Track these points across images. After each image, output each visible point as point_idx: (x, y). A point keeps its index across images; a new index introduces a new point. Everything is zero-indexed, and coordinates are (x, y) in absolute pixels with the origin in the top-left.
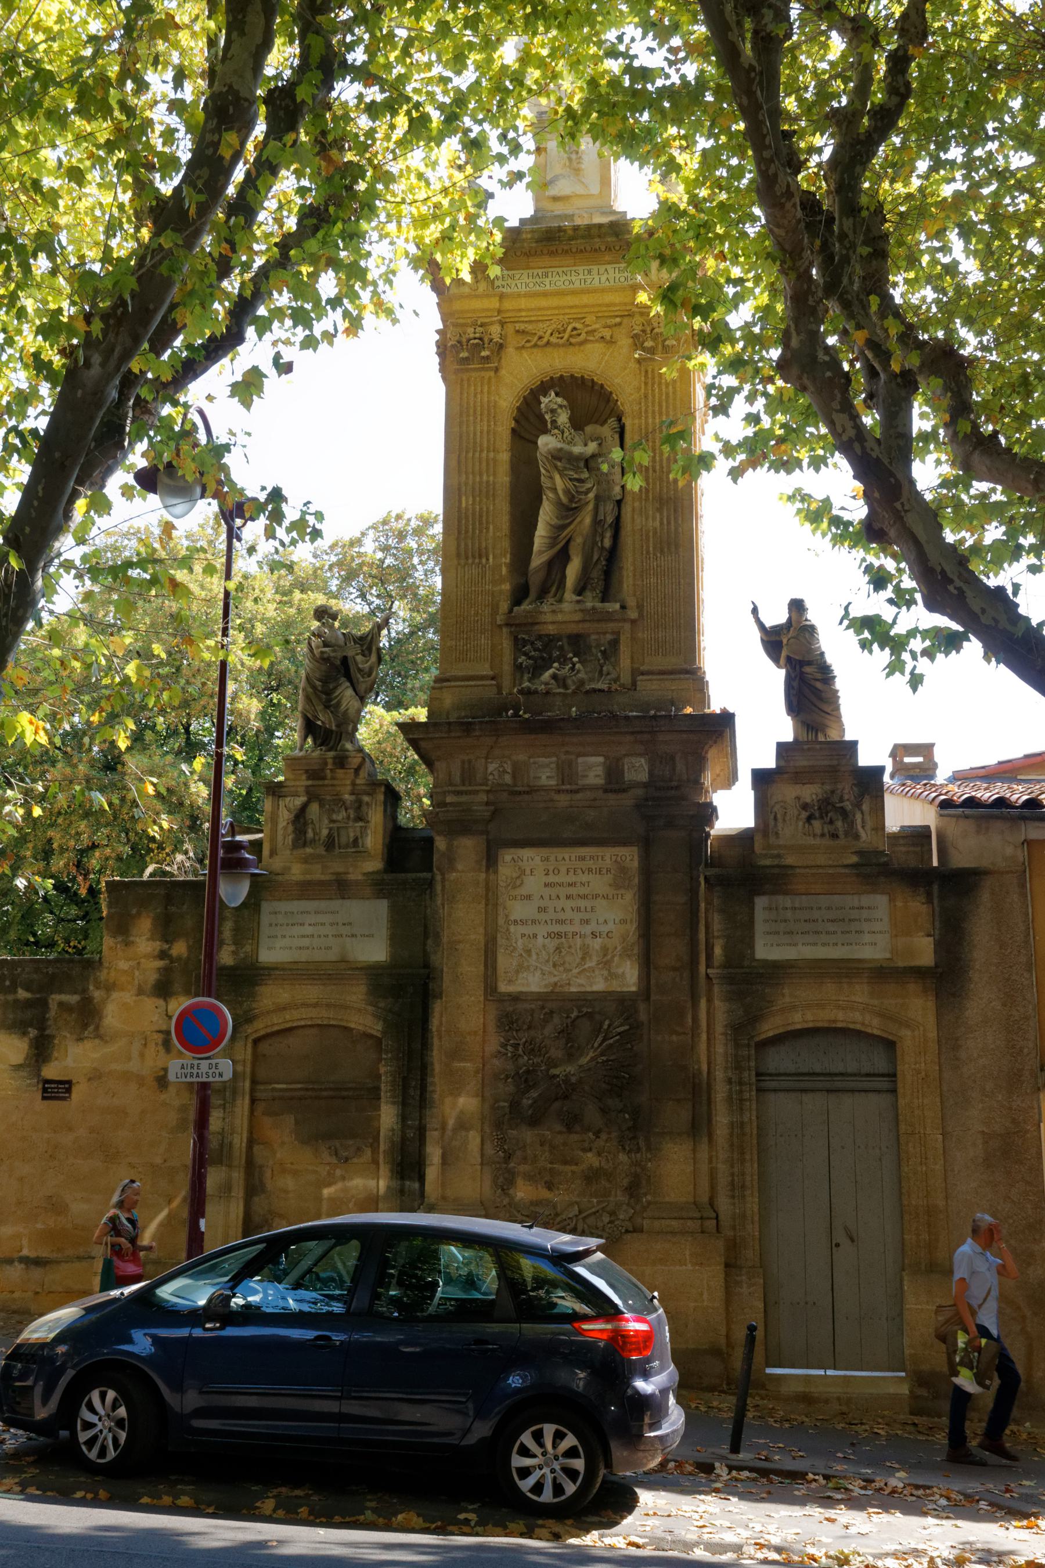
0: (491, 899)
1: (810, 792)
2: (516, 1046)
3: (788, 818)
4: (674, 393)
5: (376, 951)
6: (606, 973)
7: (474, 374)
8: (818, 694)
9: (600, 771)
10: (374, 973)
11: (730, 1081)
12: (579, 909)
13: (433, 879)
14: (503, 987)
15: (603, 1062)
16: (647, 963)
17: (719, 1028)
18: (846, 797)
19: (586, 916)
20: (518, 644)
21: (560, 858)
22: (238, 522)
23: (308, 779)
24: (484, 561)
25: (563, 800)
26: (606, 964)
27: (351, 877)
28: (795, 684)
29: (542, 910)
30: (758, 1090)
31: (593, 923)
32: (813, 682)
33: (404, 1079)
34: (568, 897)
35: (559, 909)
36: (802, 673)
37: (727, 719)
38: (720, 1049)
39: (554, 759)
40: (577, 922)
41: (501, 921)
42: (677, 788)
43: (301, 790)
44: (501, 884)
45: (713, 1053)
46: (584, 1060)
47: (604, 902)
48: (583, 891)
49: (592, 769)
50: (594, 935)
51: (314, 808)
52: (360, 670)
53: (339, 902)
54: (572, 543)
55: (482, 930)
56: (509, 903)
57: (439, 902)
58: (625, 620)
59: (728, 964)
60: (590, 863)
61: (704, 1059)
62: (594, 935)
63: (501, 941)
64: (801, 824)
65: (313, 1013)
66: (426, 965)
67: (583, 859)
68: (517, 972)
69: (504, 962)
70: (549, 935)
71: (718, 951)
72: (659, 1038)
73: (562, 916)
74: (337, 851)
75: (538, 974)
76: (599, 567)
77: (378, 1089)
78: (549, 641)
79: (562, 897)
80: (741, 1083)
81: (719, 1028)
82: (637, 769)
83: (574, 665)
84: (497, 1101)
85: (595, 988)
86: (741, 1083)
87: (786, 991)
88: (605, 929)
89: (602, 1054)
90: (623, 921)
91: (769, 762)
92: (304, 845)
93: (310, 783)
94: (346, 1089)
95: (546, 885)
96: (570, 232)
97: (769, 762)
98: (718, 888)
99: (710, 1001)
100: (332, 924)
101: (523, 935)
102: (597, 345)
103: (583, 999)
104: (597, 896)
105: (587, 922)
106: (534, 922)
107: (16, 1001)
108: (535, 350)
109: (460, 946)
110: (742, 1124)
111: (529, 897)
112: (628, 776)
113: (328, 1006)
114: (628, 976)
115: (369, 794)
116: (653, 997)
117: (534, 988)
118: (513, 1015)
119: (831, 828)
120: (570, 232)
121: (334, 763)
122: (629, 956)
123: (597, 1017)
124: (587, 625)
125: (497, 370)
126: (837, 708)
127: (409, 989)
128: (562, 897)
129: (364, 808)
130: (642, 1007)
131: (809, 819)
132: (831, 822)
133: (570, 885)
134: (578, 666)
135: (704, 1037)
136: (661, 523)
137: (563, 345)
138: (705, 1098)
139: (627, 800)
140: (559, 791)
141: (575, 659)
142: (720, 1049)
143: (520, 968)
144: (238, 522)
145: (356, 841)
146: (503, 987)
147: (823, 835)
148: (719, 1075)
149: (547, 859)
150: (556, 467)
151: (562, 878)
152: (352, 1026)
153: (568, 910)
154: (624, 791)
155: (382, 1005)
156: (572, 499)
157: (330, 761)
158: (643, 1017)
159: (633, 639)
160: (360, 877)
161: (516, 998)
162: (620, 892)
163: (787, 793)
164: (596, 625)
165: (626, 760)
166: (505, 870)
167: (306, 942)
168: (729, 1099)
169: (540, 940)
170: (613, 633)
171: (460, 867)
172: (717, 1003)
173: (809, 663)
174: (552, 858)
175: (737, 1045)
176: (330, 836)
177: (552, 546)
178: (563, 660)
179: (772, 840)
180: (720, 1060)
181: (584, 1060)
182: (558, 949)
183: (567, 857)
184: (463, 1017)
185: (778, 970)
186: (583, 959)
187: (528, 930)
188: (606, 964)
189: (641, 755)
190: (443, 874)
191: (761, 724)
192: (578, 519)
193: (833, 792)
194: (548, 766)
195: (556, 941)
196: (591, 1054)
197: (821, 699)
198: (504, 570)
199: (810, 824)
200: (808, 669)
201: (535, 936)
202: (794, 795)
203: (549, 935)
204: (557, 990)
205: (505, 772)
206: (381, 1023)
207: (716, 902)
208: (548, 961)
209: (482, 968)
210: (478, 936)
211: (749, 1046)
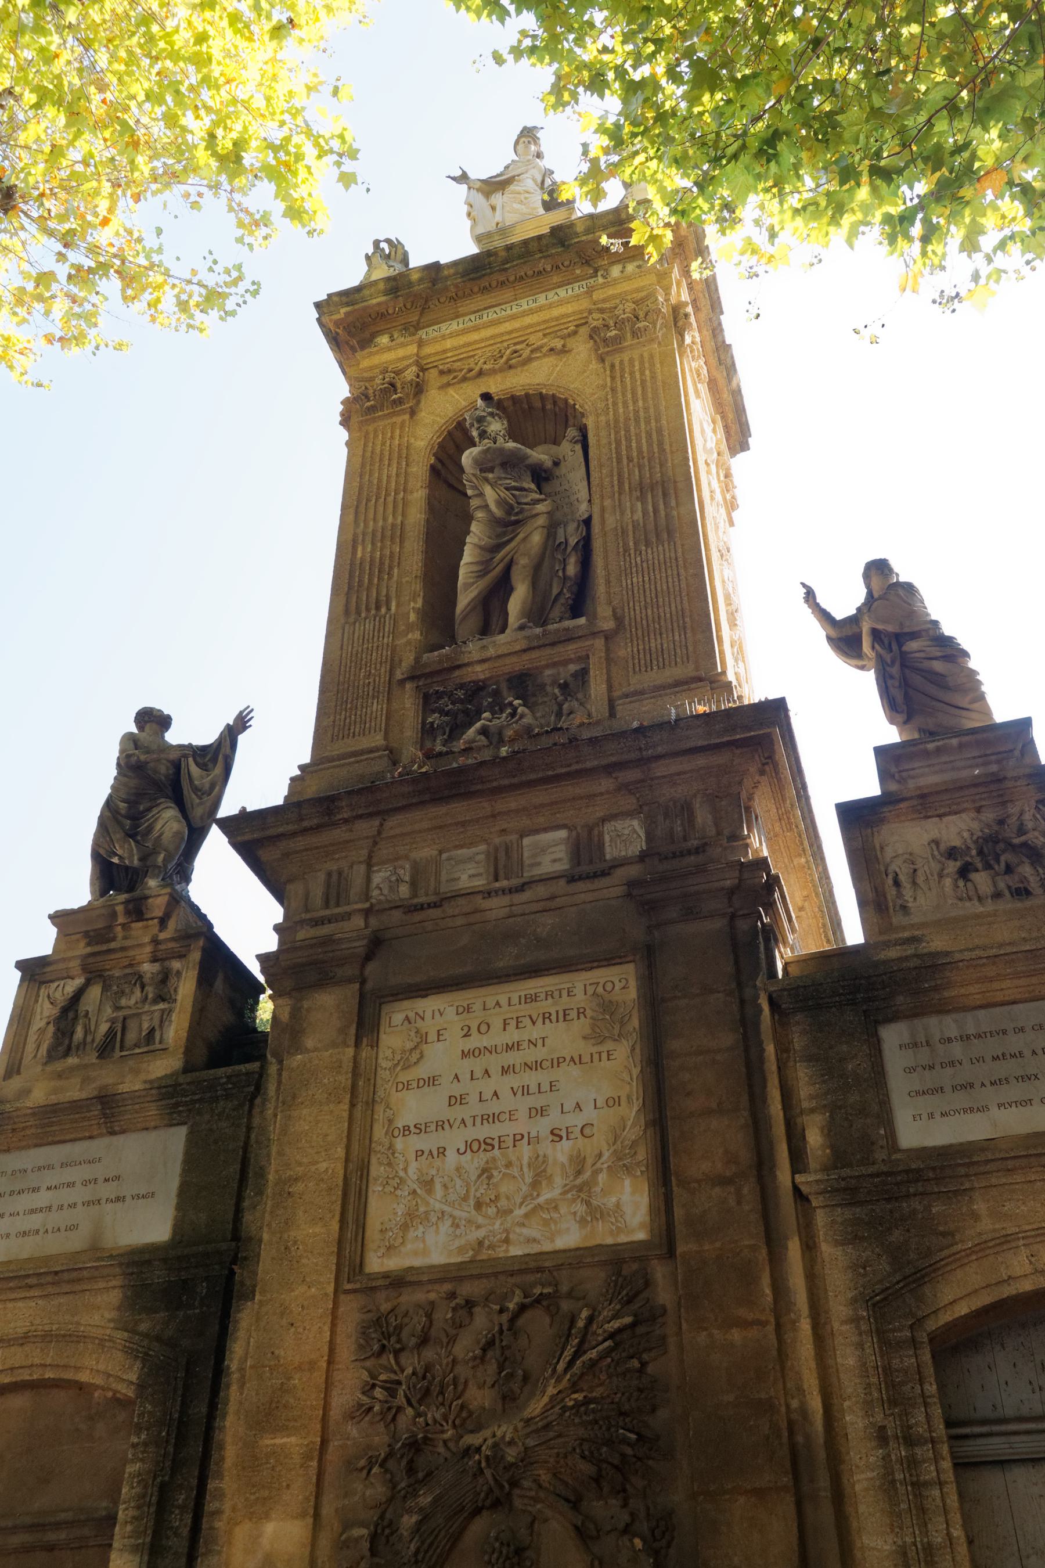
0: (361, 1094)
1: (958, 829)
2: (391, 1388)
3: (920, 880)
4: (653, 377)
5: (152, 1225)
6: (580, 1208)
7: (381, 423)
8: (939, 680)
9: (561, 852)
10: (138, 1261)
11: (881, 1437)
12: (526, 1090)
13: (262, 1073)
14: (376, 1263)
15: (578, 1405)
16: (664, 1176)
17: (839, 1309)
18: (1030, 825)
19: (538, 1101)
20: (428, 701)
21: (491, 1002)
23: (88, 944)
24: (383, 610)
25: (496, 907)
26: (582, 1190)
28: (895, 670)
29: (455, 1100)
30: (962, 1466)
31: (554, 1113)
32: (926, 664)
33: (163, 1489)
34: (505, 1071)
35: (488, 1095)
36: (903, 655)
37: (775, 712)
38: (847, 1358)
39: (483, 847)
40: (522, 1114)
41: (379, 1132)
42: (698, 851)
44: (384, 1064)
45: (831, 1363)
46: (536, 1407)
47: (575, 1071)
48: (531, 1055)
49: (549, 851)
50: (556, 1135)
52: (196, 790)
53: (106, 1140)
54: (514, 568)
55: (341, 1152)
56: (395, 1097)
58: (594, 634)
59: (839, 1158)
60: (546, 1005)
61: (811, 1382)
62: (556, 1135)
63: (377, 1170)
64: (948, 882)
68: (405, 1227)
69: (382, 1210)
70: (469, 1145)
71: (814, 1138)
72: (702, 1338)
73: (494, 1107)
74: (118, 1053)
75: (445, 1227)
76: (562, 601)
77: (111, 1519)
78: (477, 689)
79: (495, 1071)
80: (909, 1440)
81: (839, 1309)
82: (626, 837)
83: (515, 710)
84: (347, 1526)
85: (563, 1242)
86: (909, 1440)
87: (980, 1206)
88: (577, 1121)
89: (574, 1387)
90: (613, 1102)
91: (867, 785)
92: (67, 1053)
93: (89, 950)
94: (57, 1526)
95: (464, 1055)
96: (503, 254)
97: (867, 785)
98: (799, 1017)
99: (809, 1247)
100: (85, 1183)
101: (419, 1153)
102: (546, 360)
103: (535, 1266)
104: (559, 1062)
105: (542, 1111)
106: (440, 1125)
108: (464, 385)
110: (929, 1549)
111: (432, 1081)
112: (611, 852)
113: (47, 1337)
114: (630, 1210)
116: (681, 1248)
117: (438, 1257)
118: (393, 1321)
119: (1013, 881)
120: (503, 254)
121: (128, 913)
122: (627, 1169)
123: (566, 1306)
124: (535, 654)
125: (413, 413)
126: (981, 697)
128: (495, 1071)
129: (172, 981)
130: (659, 1272)
131: (964, 872)
132: (1009, 870)
133: (509, 1048)
134: (520, 710)
135: (805, 1326)
136: (645, 513)
137: (501, 370)
138: (823, 1482)
139: (611, 889)
140: (489, 894)
141: (516, 702)
142: (847, 1358)
143: (411, 1219)
146: (376, 1263)
147: (997, 895)
148: (855, 1422)
149: (468, 1009)
150: (487, 480)
151: (497, 1038)
152: (84, 1377)
153: (505, 1093)
154: (604, 874)
156: (509, 509)
157: (120, 909)
158: (664, 1295)
159: (609, 660)
161: (398, 1281)
162: (604, 1048)
163: (908, 838)
164: (548, 651)
165: (608, 827)
166: (393, 1039)
167: (35, 1221)
168: (888, 1486)
169: (451, 1156)
170: (580, 659)
172: (826, 1249)
173: (914, 636)
174: (477, 1006)
175: (886, 1345)
176: (111, 1034)
177: (482, 574)
178: (498, 706)
179: (897, 919)
180: (851, 1384)
181: (536, 1407)
182: (486, 1172)
183: (504, 1001)
184: (293, 1334)
185: (948, 1170)
186: (535, 1185)
187: (427, 1142)
188: (582, 1190)
189: (630, 814)
190: (280, 1062)
191: (842, 738)
192: (521, 536)
193: (1001, 822)
194: (471, 859)
195: (483, 1157)
196: (551, 1391)
197: (946, 688)
198: (413, 617)
199: (966, 879)
200: (913, 645)
201: (442, 1152)
202: (926, 838)
203: (469, 1145)
204: (483, 1256)
205: (400, 880)
206: (138, 1364)
207: (798, 1042)
208: (465, 1199)
209: (335, 1226)
210: (330, 1165)
211: (914, 1343)
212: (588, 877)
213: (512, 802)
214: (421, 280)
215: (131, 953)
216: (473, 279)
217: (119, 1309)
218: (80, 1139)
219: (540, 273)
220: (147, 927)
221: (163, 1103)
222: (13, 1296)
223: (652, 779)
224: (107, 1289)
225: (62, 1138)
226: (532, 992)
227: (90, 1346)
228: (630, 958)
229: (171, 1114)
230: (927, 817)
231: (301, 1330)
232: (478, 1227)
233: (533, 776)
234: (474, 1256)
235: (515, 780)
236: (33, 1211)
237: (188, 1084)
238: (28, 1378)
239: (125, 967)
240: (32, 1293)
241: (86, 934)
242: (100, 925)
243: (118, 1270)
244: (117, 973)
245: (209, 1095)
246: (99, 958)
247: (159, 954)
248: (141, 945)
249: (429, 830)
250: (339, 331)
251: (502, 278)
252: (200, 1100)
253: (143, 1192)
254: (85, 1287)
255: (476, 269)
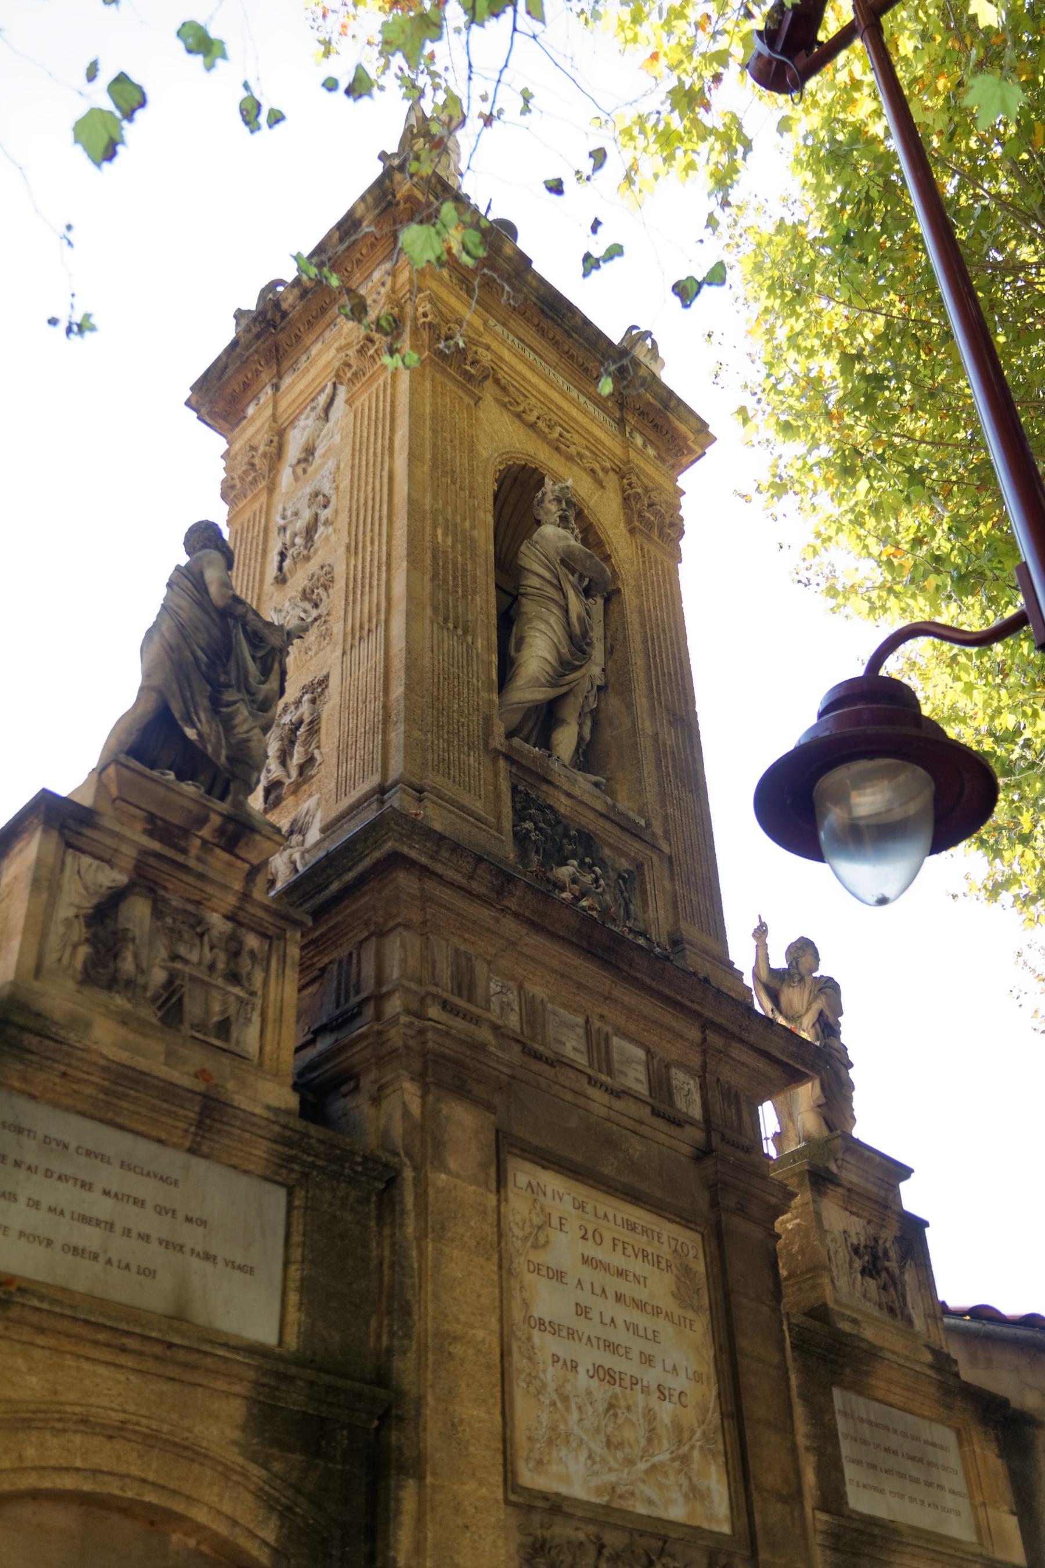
23: (150, 833)
27: (240, 1101)
43: (129, 853)
51: (138, 912)
56: (529, 1278)
57: (410, 1230)
65: (104, 1454)
66: (382, 1378)
67: (632, 1227)
75: (583, 1456)
95: (586, 1260)
100: (161, 1210)
101: (556, 1359)
109: (457, 1349)
113: (151, 1440)
115: (264, 936)
121: (221, 832)
124: (608, 825)
145: (224, 1028)
155: (277, 1466)
157: (216, 820)
160: (258, 1110)
164: (618, 832)
167: (90, 1237)
171: (453, 1164)
206: (274, 1522)
212: (668, 1120)
213: (628, 996)
214: (509, 259)
215: (210, 889)
216: (543, 311)
217: (244, 1428)
218: (147, 1137)
219: (586, 370)
220: (230, 865)
221: (280, 1148)
222: (95, 1353)
223: (727, 1056)
224: (227, 1394)
225: (127, 1123)
226: (632, 1219)
227: (209, 1472)
228: (701, 1229)
229: (281, 1166)
230: (846, 1209)
231: (476, 1537)
232: (610, 1470)
233: (666, 991)
234: (609, 1501)
235: (654, 984)
236: (85, 1219)
237: (320, 1141)
238: (117, 1492)
239: (188, 900)
240: (122, 1359)
241: (151, 818)
242: (176, 819)
243: (251, 1374)
244: (175, 903)
245: (334, 1167)
246: (165, 867)
247: (241, 914)
248: (225, 887)
249: (554, 971)
250: (402, 205)
251: (558, 337)
252: (322, 1169)
253: (239, 1261)
254: (204, 1382)
255: (552, 307)
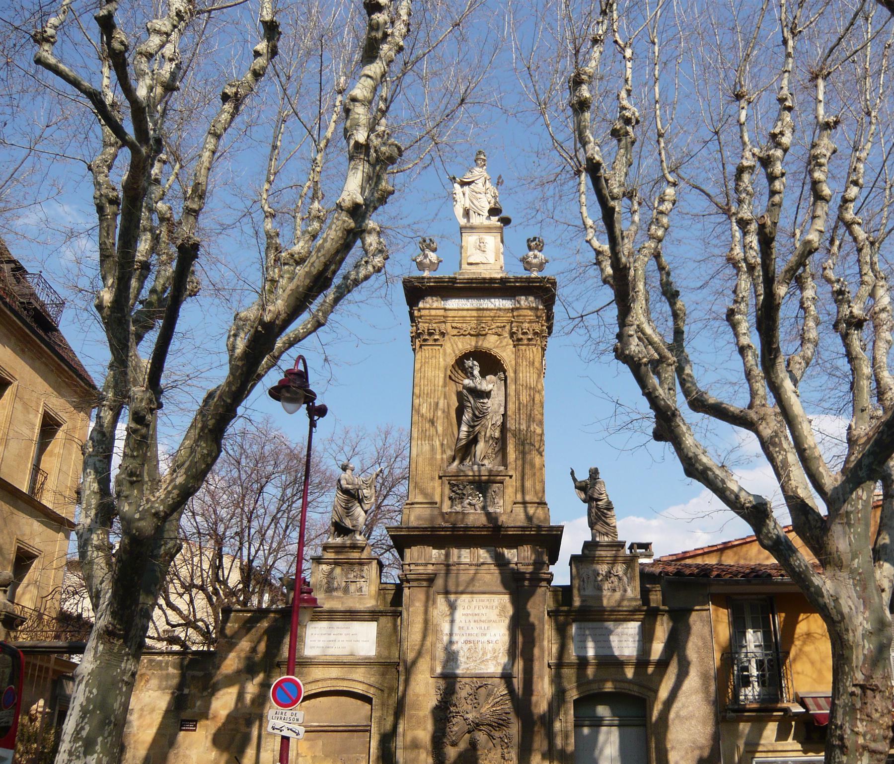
22: (316, 418)
85: (489, 671)
88: (494, 639)
89: (492, 706)
107: (168, 674)
127: (393, 668)
144: (316, 418)
195: (469, 645)
